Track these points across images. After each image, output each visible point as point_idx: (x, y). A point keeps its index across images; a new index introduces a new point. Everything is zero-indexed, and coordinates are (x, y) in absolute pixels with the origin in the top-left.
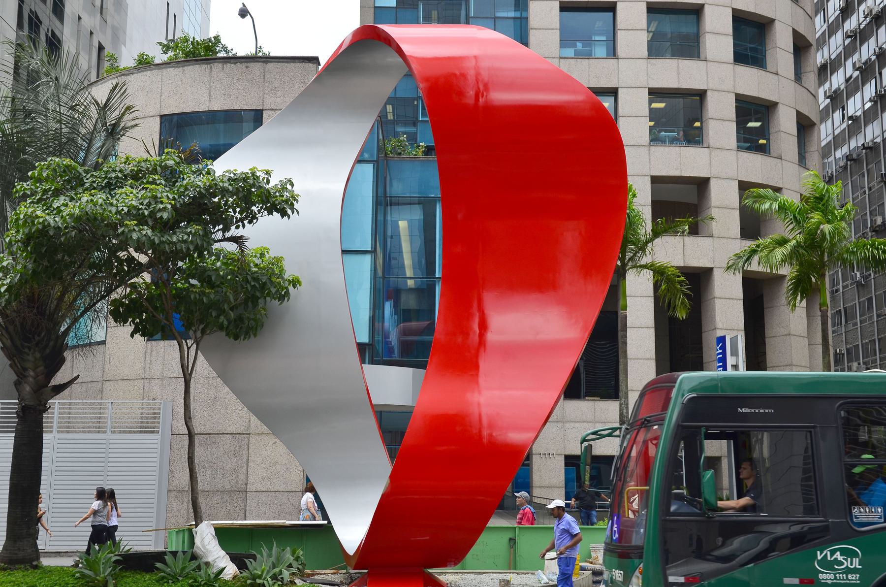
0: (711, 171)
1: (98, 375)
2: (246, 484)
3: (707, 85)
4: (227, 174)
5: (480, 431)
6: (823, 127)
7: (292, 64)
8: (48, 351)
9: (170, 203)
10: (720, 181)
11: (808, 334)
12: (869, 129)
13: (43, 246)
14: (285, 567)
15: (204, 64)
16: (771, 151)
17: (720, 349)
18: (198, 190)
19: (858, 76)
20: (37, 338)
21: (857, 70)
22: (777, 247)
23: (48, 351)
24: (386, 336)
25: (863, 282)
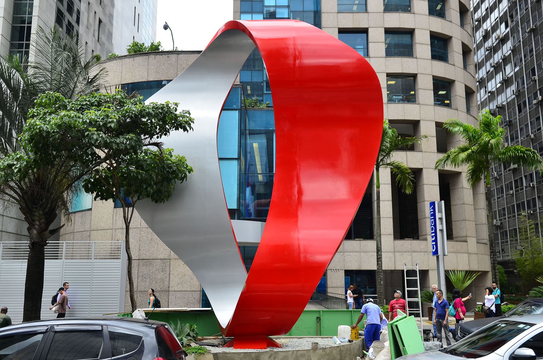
0: (420, 117)
1: (87, 227)
2: (169, 287)
3: (418, 71)
4: (152, 105)
5: (299, 255)
6: (478, 95)
7: (193, 55)
8: (47, 210)
9: (116, 119)
10: (425, 122)
11: (474, 203)
12: (499, 97)
13: (40, 143)
14: (185, 336)
15: (144, 56)
16: (452, 106)
17: (432, 209)
18: (134, 113)
19: (493, 71)
20: (41, 203)
21: (492, 67)
22: (461, 153)
23: (47, 210)
24: (247, 206)
25: (498, 177)
